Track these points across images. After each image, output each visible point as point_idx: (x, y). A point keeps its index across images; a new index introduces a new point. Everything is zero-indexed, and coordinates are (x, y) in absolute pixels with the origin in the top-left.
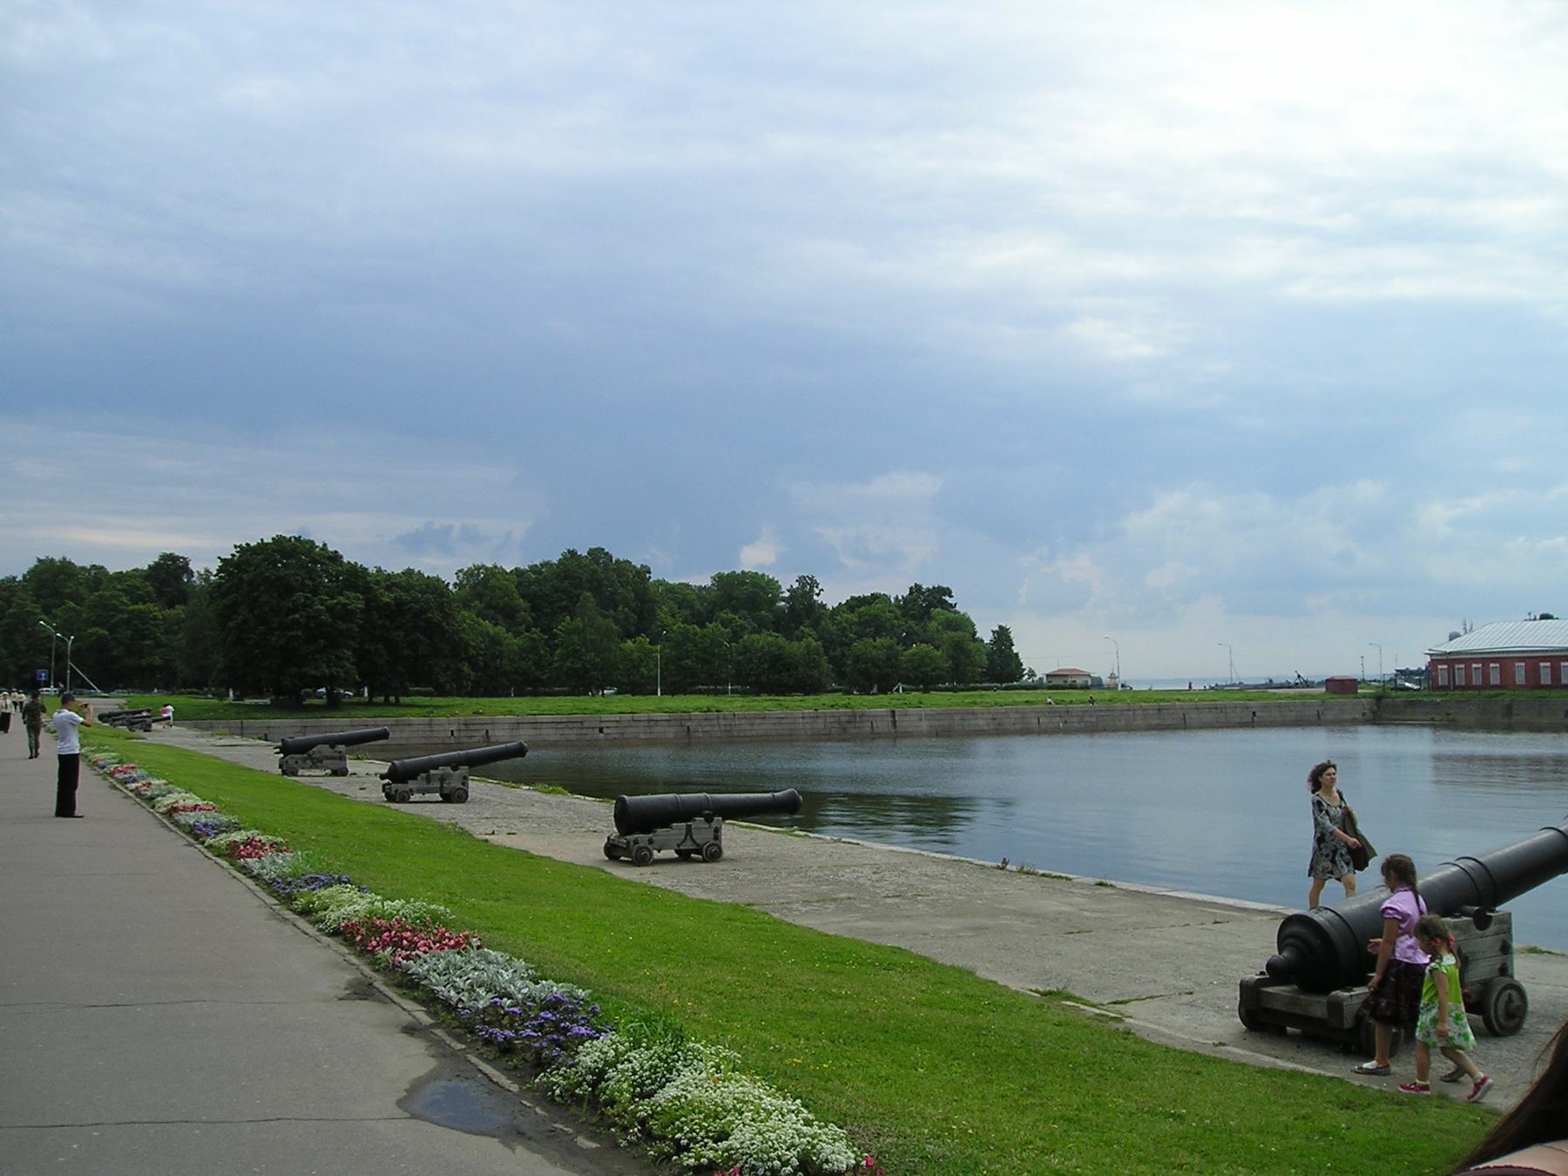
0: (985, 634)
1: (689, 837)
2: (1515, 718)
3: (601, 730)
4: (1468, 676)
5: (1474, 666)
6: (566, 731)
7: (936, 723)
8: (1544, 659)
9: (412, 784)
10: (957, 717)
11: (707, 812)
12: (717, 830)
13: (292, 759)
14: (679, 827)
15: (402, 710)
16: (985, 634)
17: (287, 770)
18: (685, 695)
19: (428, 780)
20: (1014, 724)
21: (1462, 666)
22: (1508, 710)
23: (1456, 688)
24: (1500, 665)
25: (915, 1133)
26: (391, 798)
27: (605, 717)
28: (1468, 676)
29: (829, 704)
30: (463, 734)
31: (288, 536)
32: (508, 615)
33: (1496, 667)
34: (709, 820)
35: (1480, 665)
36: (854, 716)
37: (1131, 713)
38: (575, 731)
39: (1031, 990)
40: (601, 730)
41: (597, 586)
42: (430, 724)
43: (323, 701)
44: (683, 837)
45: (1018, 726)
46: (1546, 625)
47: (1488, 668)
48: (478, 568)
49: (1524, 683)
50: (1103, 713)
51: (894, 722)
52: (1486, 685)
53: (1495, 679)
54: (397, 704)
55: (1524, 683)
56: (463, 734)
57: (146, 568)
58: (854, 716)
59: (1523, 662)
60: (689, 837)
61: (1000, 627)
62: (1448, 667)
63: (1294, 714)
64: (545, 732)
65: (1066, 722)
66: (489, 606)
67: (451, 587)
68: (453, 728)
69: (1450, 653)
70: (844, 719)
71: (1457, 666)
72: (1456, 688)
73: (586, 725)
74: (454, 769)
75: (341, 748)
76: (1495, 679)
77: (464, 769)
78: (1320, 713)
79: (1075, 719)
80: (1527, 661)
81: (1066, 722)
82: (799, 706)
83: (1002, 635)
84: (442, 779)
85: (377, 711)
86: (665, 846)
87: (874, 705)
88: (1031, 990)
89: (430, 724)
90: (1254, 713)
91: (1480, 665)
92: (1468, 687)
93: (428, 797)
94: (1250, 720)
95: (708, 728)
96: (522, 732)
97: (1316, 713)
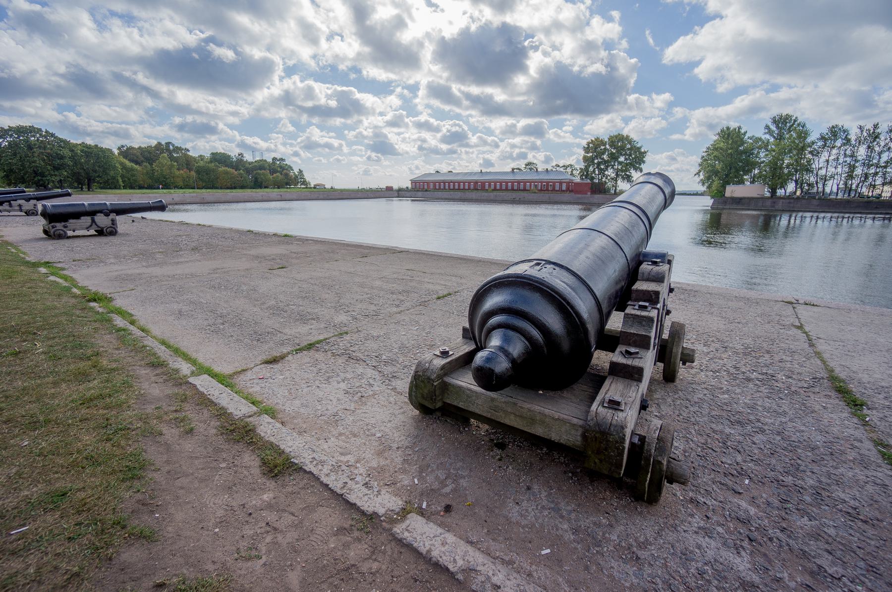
0: (296, 171)
19: (10, 205)
48: (123, 146)
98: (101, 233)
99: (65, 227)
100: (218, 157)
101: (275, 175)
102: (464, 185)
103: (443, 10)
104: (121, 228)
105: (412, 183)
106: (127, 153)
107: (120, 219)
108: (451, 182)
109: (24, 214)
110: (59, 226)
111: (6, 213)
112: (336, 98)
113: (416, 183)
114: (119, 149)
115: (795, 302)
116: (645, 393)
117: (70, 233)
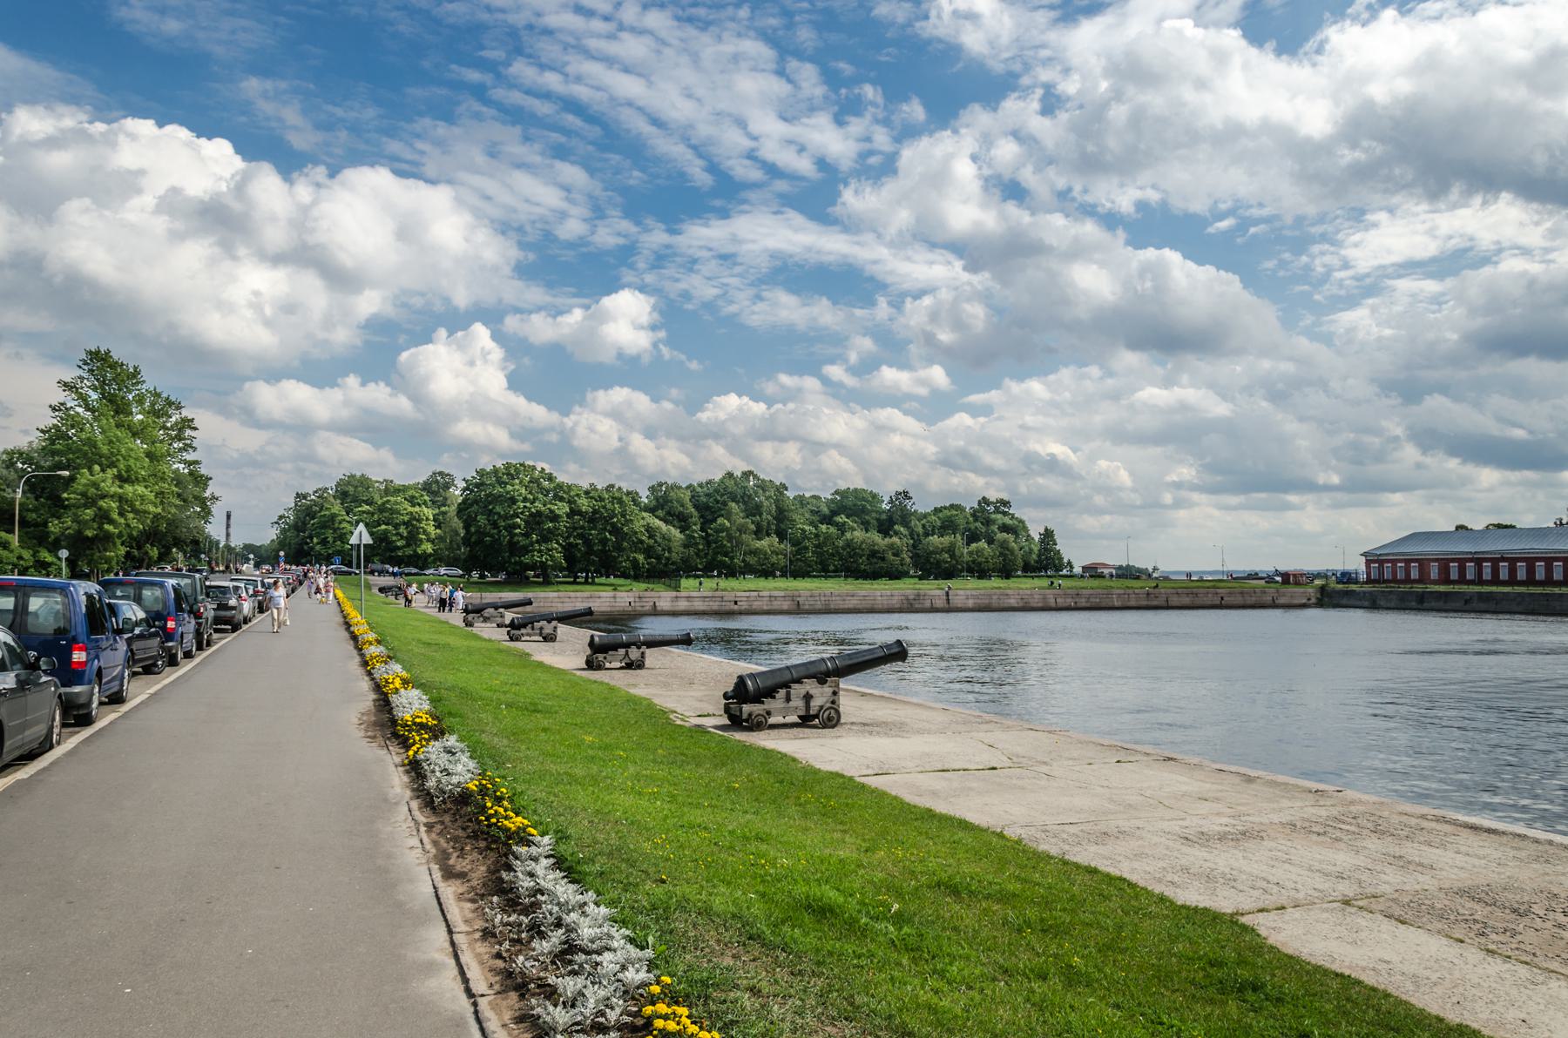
0: (1035, 532)
2: (1425, 604)
3: (736, 603)
4: (1394, 573)
5: (1399, 565)
6: (711, 603)
7: (979, 601)
9: (523, 631)
10: (995, 597)
12: (643, 653)
13: (470, 617)
14: (622, 651)
15: (595, 588)
16: (1035, 532)
17: (469, 624)
19: (533, 629)
23: (1385, 581)
25: (554, 746)
26: (512, 639)
27: (739, 594)
28: (1394, 573)
29: (906, 587)
30: (638, 604)
31: (514, 463)
32: (681, 521)
34: (639, 648)
36: (919, 595)
38: (717, 603)
39: (1203, 839)
40: (736, 603)
41: (745, 499)
42: (614, 597)
43: (583, 580)
45: (1040, 605)
48: (660, 485)
49: (1525, 578)
51: (948, 600)
52: (1408, 580)
53: (1414, 574)
54: (593, 583)
55: (1525, 578)
56: (638, 604)
57: (1104, 271)
58: (919, 595)
61: (1046, 530)
63: (1253, 599)
64: (696, 604)
66: (669, 513)
68: (632, 600)
69: (1475, 553)
70: (912, 597)
72: (1385, 581)
73: (725, 599)
75: (501, 610)
76: (1414, 574)
77: (554, 623)
79: (1083, 600)
82: (882, 590)
83: (1048, 535)
84: (541, 629)
85: (578, 587)
86: (615, 660)
87: (933, 589)
88: (1203, 839)
89: (614, 597)
92: (1395, 580)
93: (533, 638)
95: (812, 603)
96: (679, 603)
98: (629, 666)
99: (605, 658)
100: (850, 501)
101: (974, 545)
102: (1549, 569)
103: (50, 406)
104: (648, 663)
105: (1368, 563)
106: (663, 502)
107: (649, 652)
108: (1503, 559)
109: (541, 639)
110: (601, 657)
111: (528, 638)
112: (840, 175)
113: (1381, 562)
114: (652, 489)
115: (1008, 763)
116: (13, 644)
117: (608, 665)
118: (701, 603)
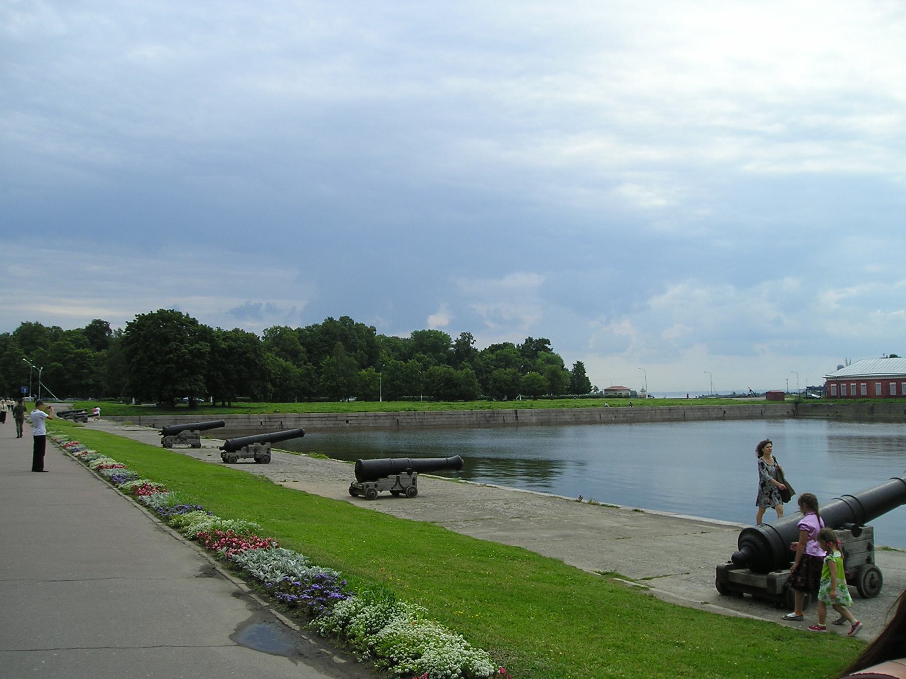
0: (569, 366)
1: (398, 483)
2: (876, 415)
3: (347, 422)
4: (848, 390)
5: (852, 384)
6: (327, 422)
7: (541, 418)
8: (892, 380)
9: (238, 453)
10: (553, 414)
11: (408, 469)
12: (414, 479)
13: (169, 438)
14: (393, 477)
15: (232, 410)
16: (569, 366)
17: (166, 445)
18: (396, 401)
19: (248, 451)
20: (586, 418)
21: (845, 385)
22: (872, 410)
24: (867, 384)
26: (226, 461)
27: (350, 414)
28: (848, 390)
29: (479, 407)
30: (267, 424)
31: (166, 310)
32: (294, 355)
33: (865, 385)
34: (410, 473)
35: (855, 384)
36: (494, 413)
37: (654, 412)
38: (332, 422)
40: (347, 422)
41: (345, 339)
42: (249, 418)
43: (187, 405)
44: (394, 483)
45: (588, 419)
46: (893, 361)
47: (860, 385)
48: (276, 328)
49: (880, 394)
50: (637, 412)
51: (517, 417)
52: (859, 396)
53: (864, 392)
54: (230, 407)
56: (267, 424)
58: (494, 413)
59: (880, 382)
60: (398, 483)
61: (578, 362)
62: (837, 385)
63: (748, 412)
64: (315, 423)
65: (616, 417)
66: (283, 350)
67: (260, 339)
69: (838, 377)
70: (488, 415)
71: (842, 385)
72: (841, 397)
73: (339, 418)
74: (263, 444)
75: (197, 432)
76: (864, 392)
77: (268, 444)
78: (763, 412)
79: (621, 415)
80: (882, 381)
81: (616, 417)
82: (461, 408)
83: (579, 367)
84: (256, 450)
85: (218, 410)
86: (384, 489)
87: (505, 407)
89: (249, 418)
90: (724, 412)
91: (855, 384)
92: (848, 397)
93: (247, 460)
94: (722, 416)
96: (302, 423)
97: (760, 411)
118: (307, 423)
